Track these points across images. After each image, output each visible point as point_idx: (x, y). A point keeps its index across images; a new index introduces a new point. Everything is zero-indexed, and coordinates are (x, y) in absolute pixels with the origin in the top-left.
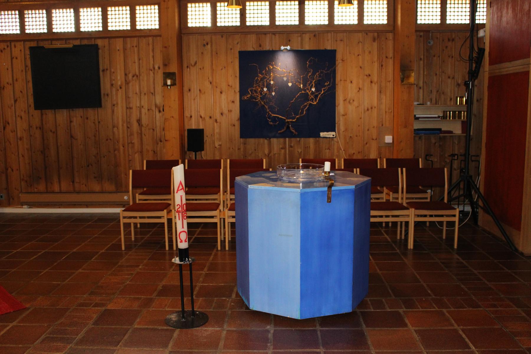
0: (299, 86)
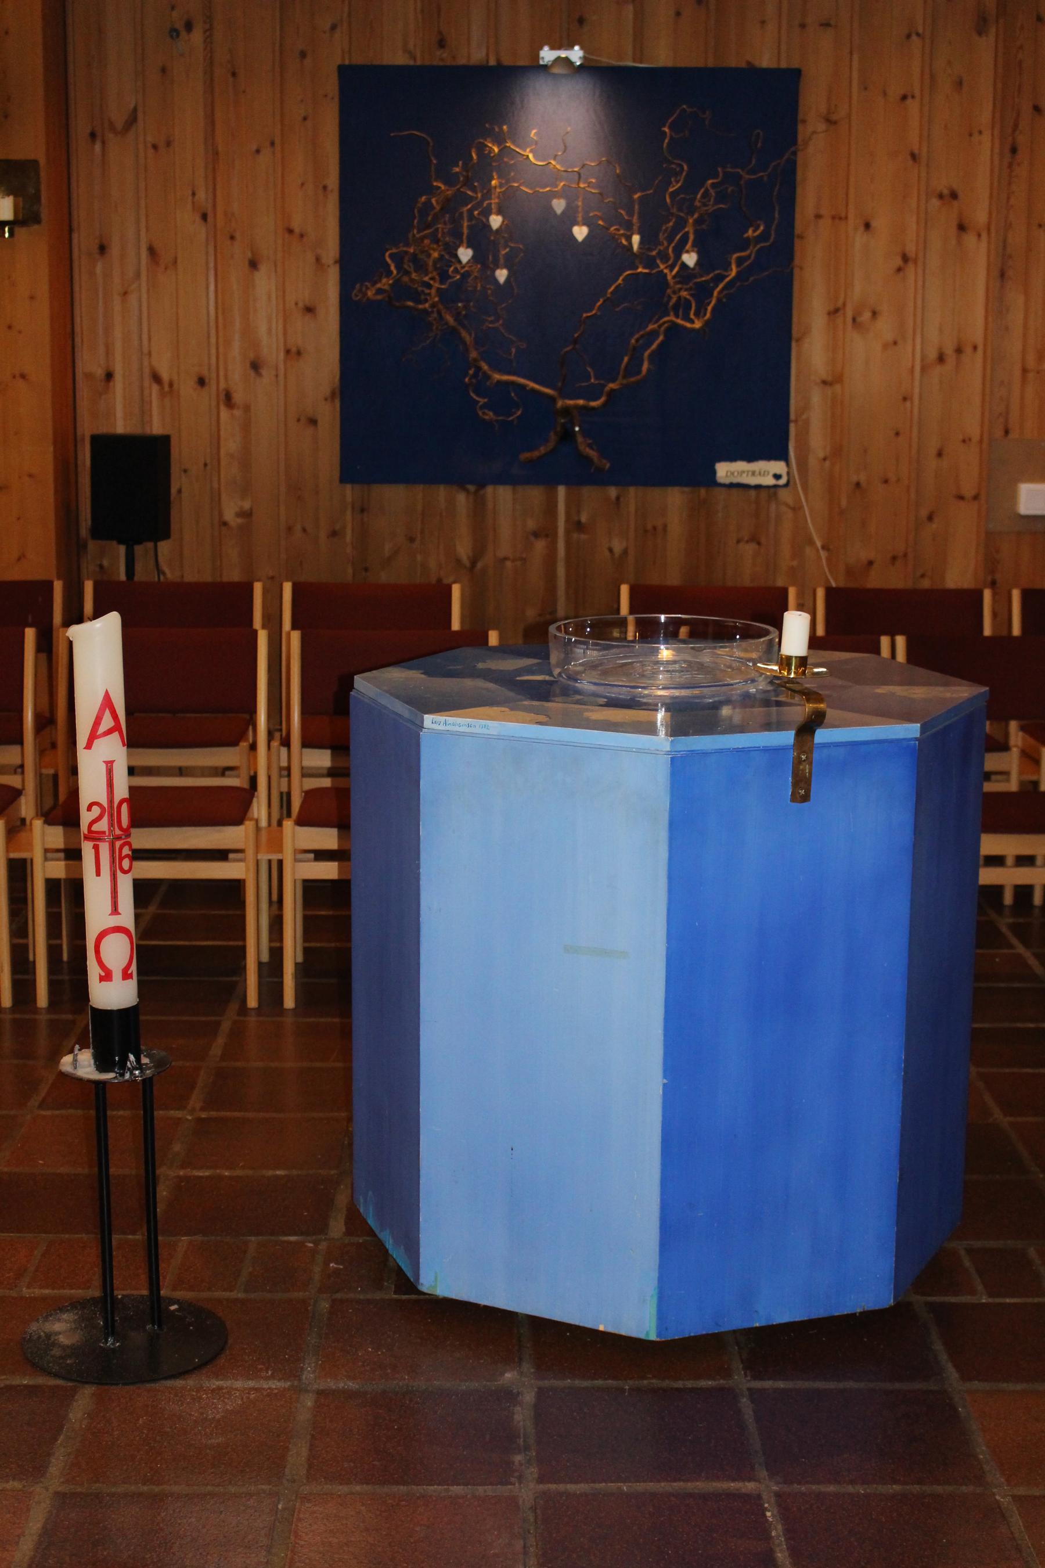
0: (624, 242)
